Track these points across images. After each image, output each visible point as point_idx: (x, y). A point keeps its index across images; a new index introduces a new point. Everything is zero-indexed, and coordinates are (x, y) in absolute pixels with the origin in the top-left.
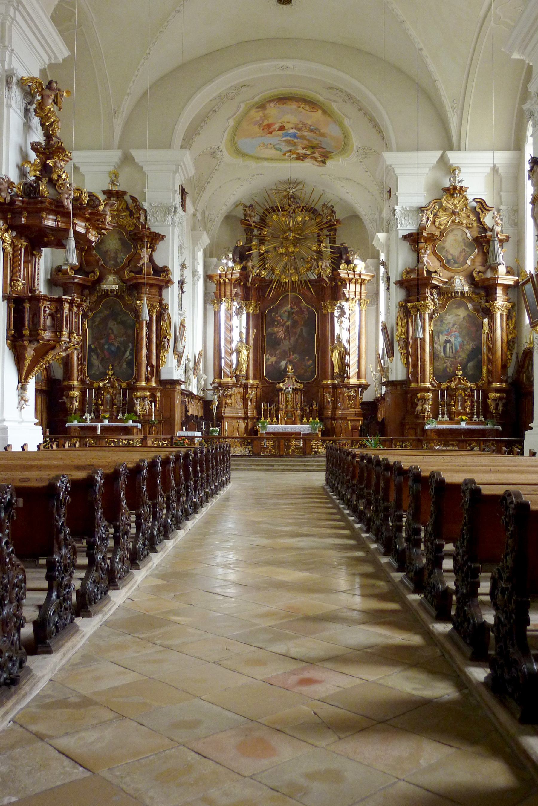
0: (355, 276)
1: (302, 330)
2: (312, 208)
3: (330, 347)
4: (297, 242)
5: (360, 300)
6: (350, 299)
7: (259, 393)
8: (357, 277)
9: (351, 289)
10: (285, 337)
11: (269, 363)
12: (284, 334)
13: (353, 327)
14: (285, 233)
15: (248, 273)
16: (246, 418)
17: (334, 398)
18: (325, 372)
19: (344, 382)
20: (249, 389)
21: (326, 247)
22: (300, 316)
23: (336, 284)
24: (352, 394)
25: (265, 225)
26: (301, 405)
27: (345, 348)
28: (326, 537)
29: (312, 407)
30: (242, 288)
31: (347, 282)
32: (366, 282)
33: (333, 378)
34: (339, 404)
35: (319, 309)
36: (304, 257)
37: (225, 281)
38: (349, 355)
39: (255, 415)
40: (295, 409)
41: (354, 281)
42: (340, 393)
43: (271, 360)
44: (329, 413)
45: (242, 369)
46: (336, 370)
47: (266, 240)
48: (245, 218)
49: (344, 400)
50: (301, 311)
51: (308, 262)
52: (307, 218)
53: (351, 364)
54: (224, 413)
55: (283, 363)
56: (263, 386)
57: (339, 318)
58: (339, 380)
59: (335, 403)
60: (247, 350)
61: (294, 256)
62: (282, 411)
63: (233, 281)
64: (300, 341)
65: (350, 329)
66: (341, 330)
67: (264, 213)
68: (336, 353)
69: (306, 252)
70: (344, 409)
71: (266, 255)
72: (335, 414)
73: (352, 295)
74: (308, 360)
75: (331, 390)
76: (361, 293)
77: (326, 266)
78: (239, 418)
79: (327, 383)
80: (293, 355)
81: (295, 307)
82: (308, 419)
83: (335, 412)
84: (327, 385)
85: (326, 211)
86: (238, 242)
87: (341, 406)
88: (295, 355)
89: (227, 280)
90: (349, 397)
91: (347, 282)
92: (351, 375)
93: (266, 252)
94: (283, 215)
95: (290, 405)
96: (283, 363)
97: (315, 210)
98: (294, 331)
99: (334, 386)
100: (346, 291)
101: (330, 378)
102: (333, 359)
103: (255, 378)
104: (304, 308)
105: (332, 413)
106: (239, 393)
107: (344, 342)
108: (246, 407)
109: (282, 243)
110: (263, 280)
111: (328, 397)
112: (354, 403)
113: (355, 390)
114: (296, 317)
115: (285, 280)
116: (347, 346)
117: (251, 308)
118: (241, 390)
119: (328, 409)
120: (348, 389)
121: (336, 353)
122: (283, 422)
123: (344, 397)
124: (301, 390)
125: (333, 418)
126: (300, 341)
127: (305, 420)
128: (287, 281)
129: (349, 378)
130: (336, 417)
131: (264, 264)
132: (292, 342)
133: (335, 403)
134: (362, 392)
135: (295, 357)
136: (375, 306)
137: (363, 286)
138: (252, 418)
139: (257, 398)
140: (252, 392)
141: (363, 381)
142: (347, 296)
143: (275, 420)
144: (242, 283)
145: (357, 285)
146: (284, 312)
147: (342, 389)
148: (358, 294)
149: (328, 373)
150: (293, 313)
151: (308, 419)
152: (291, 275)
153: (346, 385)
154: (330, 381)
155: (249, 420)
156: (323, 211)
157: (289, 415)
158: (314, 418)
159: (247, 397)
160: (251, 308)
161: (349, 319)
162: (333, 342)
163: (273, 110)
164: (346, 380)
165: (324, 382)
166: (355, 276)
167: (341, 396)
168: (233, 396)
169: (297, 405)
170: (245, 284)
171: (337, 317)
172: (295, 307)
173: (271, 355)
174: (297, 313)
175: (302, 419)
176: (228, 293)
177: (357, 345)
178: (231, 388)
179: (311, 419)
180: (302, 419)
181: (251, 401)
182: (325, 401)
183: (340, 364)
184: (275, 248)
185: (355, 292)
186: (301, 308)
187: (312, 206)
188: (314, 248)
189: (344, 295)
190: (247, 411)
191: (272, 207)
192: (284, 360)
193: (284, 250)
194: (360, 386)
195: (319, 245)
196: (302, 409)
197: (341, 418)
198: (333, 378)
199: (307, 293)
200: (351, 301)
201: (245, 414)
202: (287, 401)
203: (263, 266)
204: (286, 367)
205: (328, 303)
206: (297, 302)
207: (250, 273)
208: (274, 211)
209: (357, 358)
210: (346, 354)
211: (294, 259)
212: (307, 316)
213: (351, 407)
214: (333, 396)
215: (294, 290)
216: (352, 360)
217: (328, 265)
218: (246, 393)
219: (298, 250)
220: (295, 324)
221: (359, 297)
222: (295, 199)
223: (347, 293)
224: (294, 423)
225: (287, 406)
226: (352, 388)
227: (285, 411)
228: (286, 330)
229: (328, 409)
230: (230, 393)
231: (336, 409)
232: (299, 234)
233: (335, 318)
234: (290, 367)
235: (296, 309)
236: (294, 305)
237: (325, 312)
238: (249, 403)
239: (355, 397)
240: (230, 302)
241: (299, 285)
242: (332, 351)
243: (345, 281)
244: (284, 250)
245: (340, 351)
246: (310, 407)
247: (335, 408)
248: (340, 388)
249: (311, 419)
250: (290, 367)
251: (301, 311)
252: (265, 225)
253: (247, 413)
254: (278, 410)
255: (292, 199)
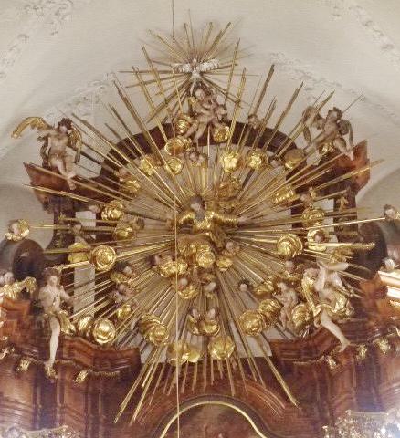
2: (269, 131)
4: (226, 235)
15: (47, 321)
21: (324, 238)
23: (373, 350)
30: (27, 386)
36: (252, 282)
47: (120, 238)
48: (45, 165)
51: (270, 295)
61: (217, 281)
67: (112, 152)
69: (257, 268)
71: (117, 278)
77: (329, 285)
85: (315, 133)
86: (15, 226)
94: (175, 152)
97: (280, 136)
109: (172, 246)
110: (104, 356)
115: (185, 357)
128: (195, 360)
131: (113, 305)
144: (25, 365)
156: (306, 132)
163: (243, 286)
170: (38, 369)
184: (150, 261)
187: (271, 125)
188: (285, 248)
191: (139, 138)
193: (181, 268)
195: (303, 236)
203: (107, 310)
207: (54, 322)
208: (148, 150)
211: (218, 290)
215: (219, 387)
217: (338, 282)
219: (228, 262)
222: (208, 93)
244: (181, 268)
252: (116, 187)
255: (199, 93)
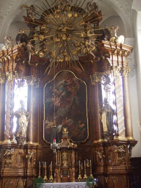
0: (116, 47)
1: (74, 99)
2: (79, 8)
3: (99, 110)
4: (69, 33)
5: (122, 68)
6: (114, 67)
7: (39, 154)
8: (118, 48)
9: (113, 60)
10: (60, 105)
11: (48, 127)
12: (60, 102)
13: (118, 90)
14: (59, 27)
15: (28, 52)
16: (25, 177)
17: (105, 155)
18: (96, 133)
19: (113, 139)
20: (29, 150)
22: (72, 87)
23: (101, 59)
24: (121, 150)
25: (44, 21)
26: (75, 163)
27: (112, 109)
28: (123, 94)
29: (86, 164)
31: (110, 53)
32: (126, 53)
33: (103, 137)
34: (110, 161)
35: (88, 82)
37: (8, 58)
38: (116, 114)
39: (34, 173)
40: (70, 167)
41: (116, 52)
42: (110, 151)
43: (49, 125)
44: (101, 170)
45: (21, 132)
46: (105, 129)
48: (28, 16)
49: (114, 157)
50: (73, 84)
51: (78, 46)
52: (76, 15)
53: (118, 122)
54: (3, 173)
55: (60, 126)
56: (43, 148)
57: (105, 84)
58: (108, 138)
59: (106, 159)
60: (27, 116)
62: (58, 169)
63: (14, 58)
64: (73, 108)
65: (116, 92)
66: (107, 95)
67: (43, 13)
68: (104, 115)
70: (114, 165)
71: (44, 42)
72: (107, 170)
73: (115, 64)
74: (81, 124)
75: (102, 148)
76: (122, 62)
77: (92, 44)
78: (18, 177)
79: (98, 142)
80: (68, 120)
81: (69, 81)
82: (83, 176)
83: (107, 168)
84: (98, 144)
87: (112, 163)
88: (70, 120)
89: (9, 57)
90: (119, 153)
91: (110, 53)
92: (119, 133)
93: (45, 40)
94: (57, 13)
95: (65, 165)
96: (60, 126)
97: (82, 9)
98: (68, 100)
99: (105, 145)
100: (110, 60)
101: (100, 137)
102: (102, 121)
103: (34, 141)
104: (76, 81)
105: (104, 170)
106: (20, 153)
107: (111, 104)
108: (26, 168)
111: (100, 155)
112: (123, 159)
113: (125, 147)
114: (70, 89)
115: (60, 60)
116: (114, 107)
117: (32, 82)
118: (22, 151)
119: (100, 166)
120: (118, 146)
121: (104, 115)
122: (59, 180)
123: (114, 153)
124: (75, 150)
125: (105, 174)
126: (73, 108)
127: (80, 177)
128: (62, 61)
129: (117, 135)
130: (108, 173)
132: (66, 109)
133: (106, 159)
134: (130, 149)
135: (69, 121)
136: (135, 76)
137: (124, 58)
138: (32, 177)
139: (37, 158)
140: (31, 152)
141: (131, 138)
142: (111, 65)
143: (51, 178)
144: (24, 62)
145: (119, 57)
146: (60, 85)
147: (112, 147)
148: (120, 63)
149: (98, 133)
150: (67, 86)
151: (83, 176)
152: (65, 56)
153: (115, 142)
154: (100, 140)
155: (28, 179)
157: (65, 172)
158: (88, 175)
159: (27, 157)
160: (32, 82)
161: (114, 84)
162: (101, 106)
164: (115, 138)
165: (95, 142)
166: (116, 47)
167: (111, 153)
168: (13, 157)
169: (71, 163)
170: (26, 63)
171: (103, 85)
172: (69, 81)
173: (50, 121)
174: (70, 85)
175: (76, 177)
176: (10, 68)
177: (122, 95)
178: (10, 149)
179: (85, 176)
180: (76, 177)
181: (31, 161)
182: (97, 159)
183: (108, 124)
184: (52, 38)
185: (118, 61)
186: (73, 82)
187: (80, 6)
189: (109, 64)
190: (27, 170)
191: (49, 10)
192: (61, 124)
193: (59, 40)
194: (128, 142)
195: (86, 33)
196: (77, 167)
197: (113, 175)
198: (103, 137)
199: (78, 69)
200: (114, 69)
201: (24, 173)
202: (62, 160)
204: (62, 130)
205: (95, 74)
206: (70, 76)
207: (30, 52)
209: (123, 118)
210: (114, 114)
211: (67, 45)
212: (79, 88)
213: (121, 163)
214: (104, 153)
215: (67, 67)
216: (119, 118)
217: (94, 43)
218: (27, 153)
220: (69, 94)
221: (121, 66)
223: (110, 62)
224: (69, 180)
225: (62, 164)
226: (121, 144)
227: (61, 169)
228: (61, 100)
229: (100, 166)
230: (9, 153)
231: (108, 165)
232: (70, 27)
233: (102, 85)
234: (65, 130)
235: (69, 82)
236: (68, 79)
237: (93, 83)
238: (29, 163)
239: (123, 153)
240: (12, 75)
241: (71, 64)
242: (101, 114)
243: (108, 53)
245: (108, 113)
246: (84, 164)
247: (106, 166)
248: (110, 146)
249: (85, 176)
250: (65, 130)
251: (73, 84)
252: (44, 21)
253: (27, 172)
254: (54, 167)
